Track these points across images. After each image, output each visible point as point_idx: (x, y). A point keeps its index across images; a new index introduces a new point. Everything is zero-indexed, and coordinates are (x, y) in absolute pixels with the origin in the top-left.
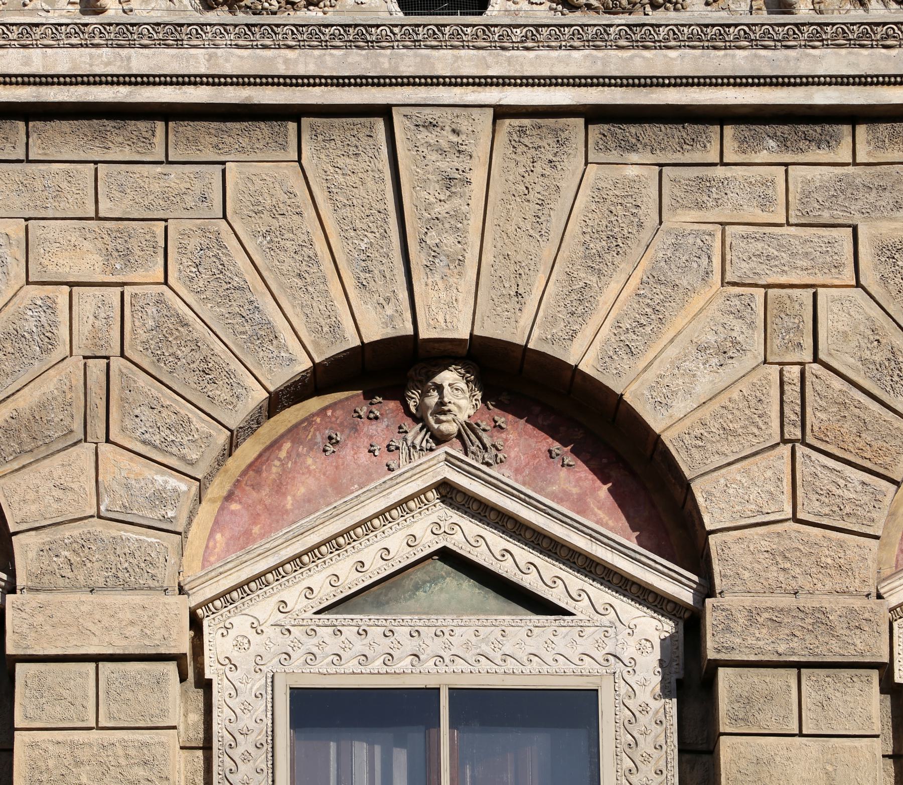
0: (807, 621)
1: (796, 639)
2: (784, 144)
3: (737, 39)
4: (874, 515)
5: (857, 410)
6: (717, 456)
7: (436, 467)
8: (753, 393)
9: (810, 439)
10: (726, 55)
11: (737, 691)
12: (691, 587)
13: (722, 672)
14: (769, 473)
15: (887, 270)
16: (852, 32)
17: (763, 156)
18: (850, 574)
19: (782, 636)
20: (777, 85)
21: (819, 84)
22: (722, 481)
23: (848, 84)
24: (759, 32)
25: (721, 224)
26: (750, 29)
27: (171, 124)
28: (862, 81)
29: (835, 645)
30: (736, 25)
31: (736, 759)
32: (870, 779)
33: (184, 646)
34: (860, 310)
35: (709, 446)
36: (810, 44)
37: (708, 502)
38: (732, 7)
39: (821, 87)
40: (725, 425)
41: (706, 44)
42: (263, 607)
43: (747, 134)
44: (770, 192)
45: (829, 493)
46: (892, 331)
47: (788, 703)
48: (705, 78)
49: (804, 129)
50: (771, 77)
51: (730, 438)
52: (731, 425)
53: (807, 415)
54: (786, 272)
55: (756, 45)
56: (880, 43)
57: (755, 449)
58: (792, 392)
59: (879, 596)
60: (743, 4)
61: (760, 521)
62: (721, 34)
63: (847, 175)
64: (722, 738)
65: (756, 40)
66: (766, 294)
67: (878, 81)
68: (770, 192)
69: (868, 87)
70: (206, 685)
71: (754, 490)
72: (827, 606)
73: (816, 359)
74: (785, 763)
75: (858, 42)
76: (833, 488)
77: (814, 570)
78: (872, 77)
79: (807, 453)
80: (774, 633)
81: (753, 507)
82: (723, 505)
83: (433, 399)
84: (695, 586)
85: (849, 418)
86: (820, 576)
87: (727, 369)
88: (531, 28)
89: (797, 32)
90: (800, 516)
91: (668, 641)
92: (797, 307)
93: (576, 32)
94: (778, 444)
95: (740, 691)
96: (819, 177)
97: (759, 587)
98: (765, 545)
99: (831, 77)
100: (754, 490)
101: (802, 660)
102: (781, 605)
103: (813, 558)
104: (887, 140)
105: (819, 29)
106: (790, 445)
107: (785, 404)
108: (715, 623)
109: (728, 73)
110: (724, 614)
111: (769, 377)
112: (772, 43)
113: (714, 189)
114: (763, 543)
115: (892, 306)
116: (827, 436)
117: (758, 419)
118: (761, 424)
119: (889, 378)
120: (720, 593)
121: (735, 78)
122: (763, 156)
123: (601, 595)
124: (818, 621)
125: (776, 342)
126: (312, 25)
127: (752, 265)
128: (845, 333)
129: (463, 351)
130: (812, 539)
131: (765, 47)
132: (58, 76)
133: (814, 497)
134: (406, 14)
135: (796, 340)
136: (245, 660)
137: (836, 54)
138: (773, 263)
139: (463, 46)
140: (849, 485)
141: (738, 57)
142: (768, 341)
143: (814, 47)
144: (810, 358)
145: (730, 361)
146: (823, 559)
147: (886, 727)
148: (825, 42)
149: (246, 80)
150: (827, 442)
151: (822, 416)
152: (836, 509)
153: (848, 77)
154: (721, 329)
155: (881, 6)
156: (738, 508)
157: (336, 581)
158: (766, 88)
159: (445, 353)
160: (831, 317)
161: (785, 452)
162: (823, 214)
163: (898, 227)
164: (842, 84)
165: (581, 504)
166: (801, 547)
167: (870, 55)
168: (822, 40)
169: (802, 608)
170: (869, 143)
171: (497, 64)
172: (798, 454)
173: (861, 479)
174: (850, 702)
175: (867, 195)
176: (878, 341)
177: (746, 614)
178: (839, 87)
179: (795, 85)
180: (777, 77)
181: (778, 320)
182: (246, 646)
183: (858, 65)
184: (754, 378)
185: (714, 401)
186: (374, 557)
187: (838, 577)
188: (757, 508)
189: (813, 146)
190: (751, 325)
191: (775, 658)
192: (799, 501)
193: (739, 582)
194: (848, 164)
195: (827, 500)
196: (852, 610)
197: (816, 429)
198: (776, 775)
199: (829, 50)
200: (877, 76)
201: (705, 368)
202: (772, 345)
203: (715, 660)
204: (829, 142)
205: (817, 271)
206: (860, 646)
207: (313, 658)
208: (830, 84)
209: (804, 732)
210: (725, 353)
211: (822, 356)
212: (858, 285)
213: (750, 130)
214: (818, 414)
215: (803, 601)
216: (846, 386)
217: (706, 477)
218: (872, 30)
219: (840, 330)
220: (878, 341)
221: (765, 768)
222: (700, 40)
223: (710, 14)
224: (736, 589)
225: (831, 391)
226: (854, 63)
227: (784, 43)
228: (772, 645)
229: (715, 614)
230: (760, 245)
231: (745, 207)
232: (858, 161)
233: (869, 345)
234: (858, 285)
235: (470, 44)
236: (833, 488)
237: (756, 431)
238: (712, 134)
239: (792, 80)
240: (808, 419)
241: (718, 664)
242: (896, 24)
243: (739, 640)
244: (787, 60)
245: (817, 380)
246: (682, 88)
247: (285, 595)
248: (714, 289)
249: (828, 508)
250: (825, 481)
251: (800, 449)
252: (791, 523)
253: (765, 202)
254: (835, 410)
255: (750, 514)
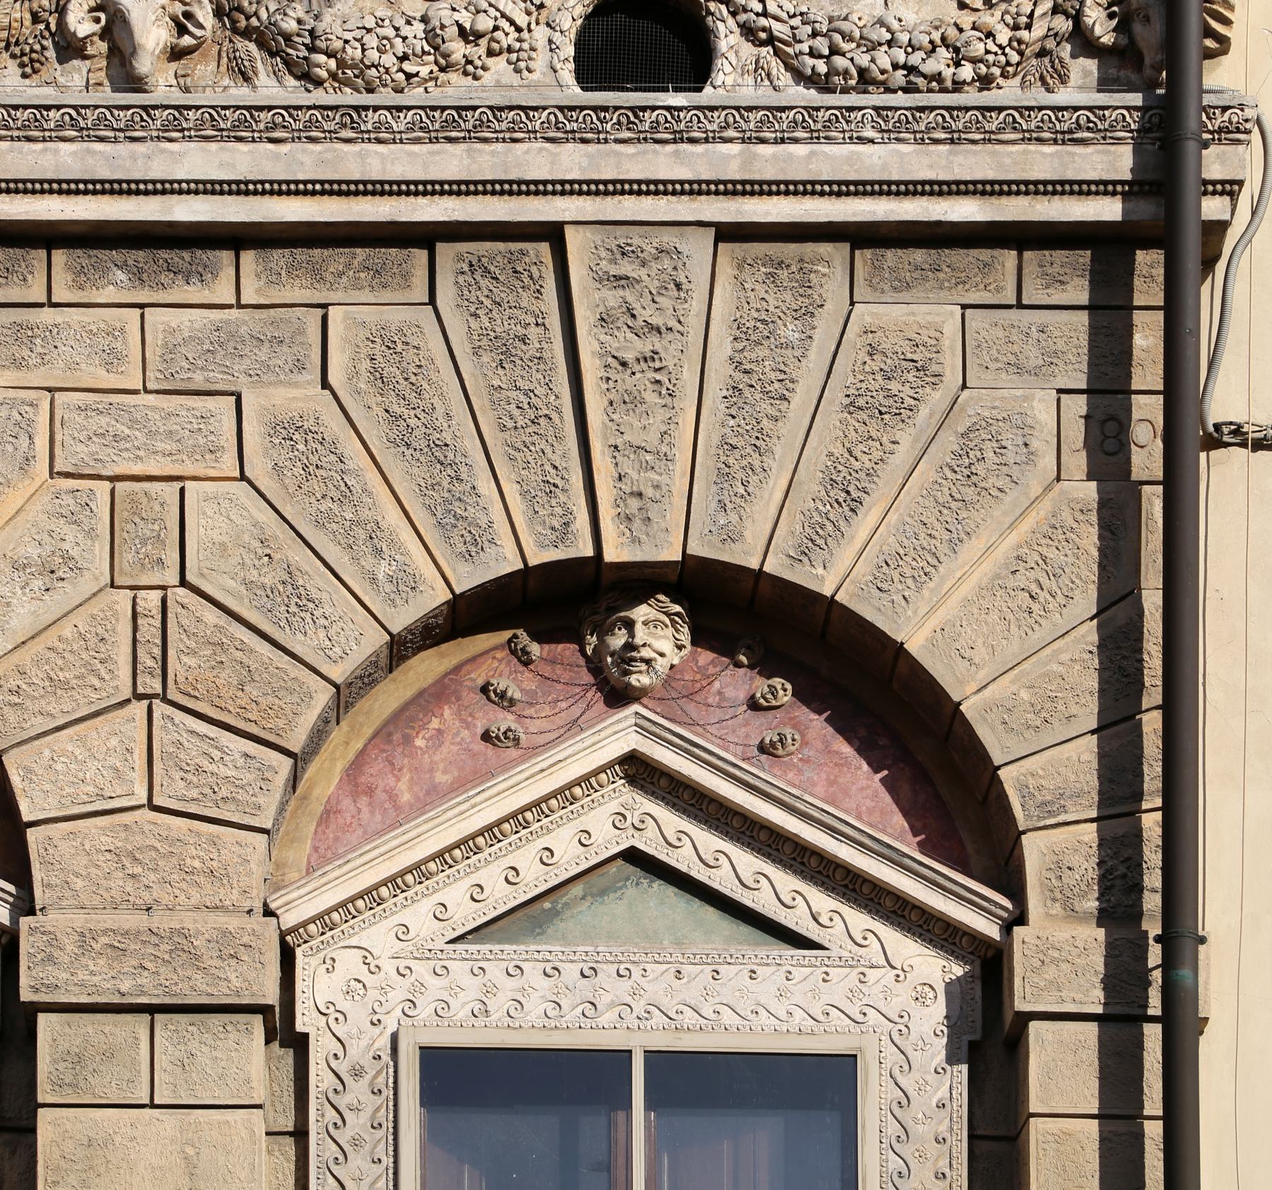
0: (162, 947)
1: (146, 973)
2: (139, 276)
3: (60, 126)
4: (261, 800)
5: (239, 654)
6: (40, 718)
7: (619, 734)
8: (93, 630)
9: (173, 694)
10: (45, 150)
11: (64, 1045)
12: (6, 901)
13: (43, 1019)
14: (114, 742)
15: (282, 456)
16: (225, 119)
17: (108, 294)
18: (225, 882)
19: (126, 969)
20: (121, 192)
21: (181, 192)
22: (47, 753)
23: (222, 193)
24: (91, 116)
25: (49, 390)
26: (79, 114)
27: (1028, 255)
28: (240, 188)
29: (200, 980)
30: (58, 107)
31: (59, 1140)
32: (245, 1165)
33: (271, 995)
34: (245, 513)
35: (28, 703)
36: (166, 135)
37: (27, 782)
38: (61, 80)
39: (184, 197)
40: (52, 675)
41: (16, 133)
42: (377, 935)
43: (85, 262)
44: (118, 345)
45: (199, 770)
46: (289, 542)
47: (134, 1062)
48: (16, 181)
49: (166, 256)
50: (111, 182)
51: (59, 692)
52: (60, 674)
53: (169, 660)
54: (141, 459)
55: (88, 136)
56: (264, 135)
57: (94, 708)
58: (149, 629)
59: (268, 913)
60: (76, 76)
61: (100, 808)
62: (37, 120)
63: (227, 322)
64: (40, 1111)
65: (88, 129)
66: (113, 492)
67: (580, 190)
68: (118, 345)
69: (251, 198)
70: (299, 1044)
71: (93, 765)
72: (191, 926)
73: (183, 582)
74: (129, 1144)
75: (232, 134)
76: (205, 764)
77: (175, 876)
78: (255, 183)
79: (168, 713)
80: (115, 964)
81: (91, 789)
82: (47, 787)
83: (618, 640)
84: (11, 899)
85: (226, 664)
86: (184, 885)
87: (56, 596)
88: (1048, 112)
89: (145, 117)
90: (157, 801)
91: (957, 988)
92: (157, 508)
93: (1046, 118)
94: (129, 701)
95: (67, 1045)
96: (188, 324)
97: (96, 901)
98: (106, 841)
99: (197, 182)
100: (93, 765)
101: (154, 1002)
102: (126, 926)
103: (174, 860)
104: (283, 273)
105: (176, 114)
106: (145, 703)
107: (138, 645)
108: (32, 951)
109: (49, 176)
110: (45, 938)
111: (117, 607)
112: (111, 134)
113: (38, 341)
114: (103, 839)
115: (289, 508)
116: (195, 689)
117: (99, 666)
118: (103, 673)
119: (283, 608)
120: (41, 910)
121: (59, 182)
122: (108, 294)
123: (859, 920)
124: (178, 948)
125: (126, 557)
126: (900, 108)
127: (93, 448)
128: (222, 544)
129: (673, 577)
130: (174, 834)
131: (102, 139)
132: (761, 183)
133: (178, 775)
134: (582, 88)
135: (156, 554)
136: (358, 1014)
137: (203, 150)
138: (123, 445)
139: (638, 139)
140: (227, 758)
141: (62, 153)
142: (116, 555)
143: (171, 140)
144: (175, 580)
145: (60, 584)
146: (188, 861)
147: (286, 1093)
148: (186, 133)
149: (601, 187)
150: (196, 697)
151: (192, 661)
152: (207, 791)
153: (221, 183)
154: (46, 539)
155: (274, 82)
156: (68, 790)
157: (495, 900)
158: (106, 198)
159: (641, 582)
160: (203, 522)
161: (137, 711)
162: (194, 376)
163: (297, 395)
164: (213, 193)
165: (840, 793)
166: (158, 845)
167: (250, 152)
168: (182, 130)
169: (155, 930)
170: (258, 276)
171: (728, 160)
172: (156, 715)
173: (244, 749)
174: (222, 1060)
175: (256, 351)
176: (269, 555)
177: (77, 938)
178: (210, 197)
179: (146, 193)
180: (120, 182)
181: (130, 527)
182: (361, 992)
183: (234, 166)
184: (94, 608)
185: (37, 640)
186: (528, 866)
187: (209, 886)
188: (96, 791)
189: (180, 280)
190: (91, 533)
191: (116, 999)
192: (157, 780)
193: (68, 894)
194: (230, 306)
195: (195, 779)
196: (225, 933)
197: (181, 679)
198: (114, 1161)
199: (192, 145)
200: (262, 182)
201: (24, 594)
202: (121, 562)
203: (32, 1003)
204: (200, 275)
205: (185, 457)
206: (236, 983)
207: (519, 1007)
208: (197, 192)
209: (157, 1101)
210: (52, 572)
211: (190, 577)
212: (243, 477)
213: (90, 256)
214: (185, 659)
215: (160, 921)
216: (223, 620)
217: (24, 747)
218: (252, 116)
219: (216, 540)
220: (269, 555)
221: (100, 1152)
222: (8, 128)
223: (29, 91)
224: (65, 903)
225: (202, 627)
226: (228, 164)
227: (128, 134)
228: (113, 982)
229: (32, 939)
230: (104, 420)
231: (83, 366)
232: (243, 302)
233: (256, 562)
234: (243, 477)
235: (649, 135)
236: (205, 764)
237: (96, 682)
238: (35, 262)
239: (142, 187)
240: (169, 665)
241: (36, 1008)
242: (286, 108)
243: (65, 976)
244: (133, 157)
245: (184, 612)
246: (19, 196)
247: (405, 916)
248: (38, 482)
249: (197, 791)
250: (193, 752)
251: (160, 708)
252: (146, 811)
253: (112, 359)
254: (208, 652)
255: (86, 798)
